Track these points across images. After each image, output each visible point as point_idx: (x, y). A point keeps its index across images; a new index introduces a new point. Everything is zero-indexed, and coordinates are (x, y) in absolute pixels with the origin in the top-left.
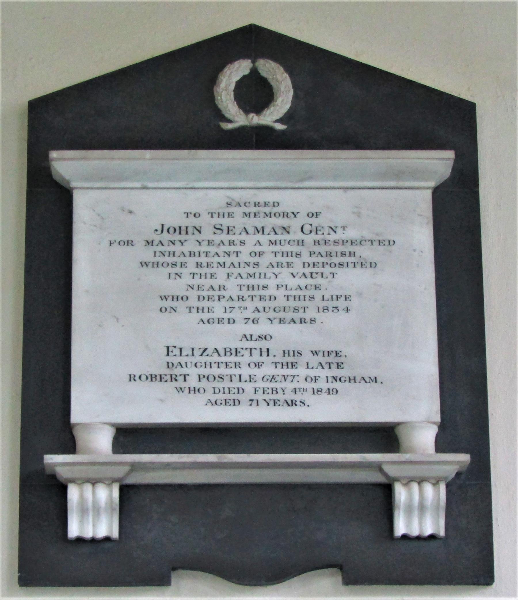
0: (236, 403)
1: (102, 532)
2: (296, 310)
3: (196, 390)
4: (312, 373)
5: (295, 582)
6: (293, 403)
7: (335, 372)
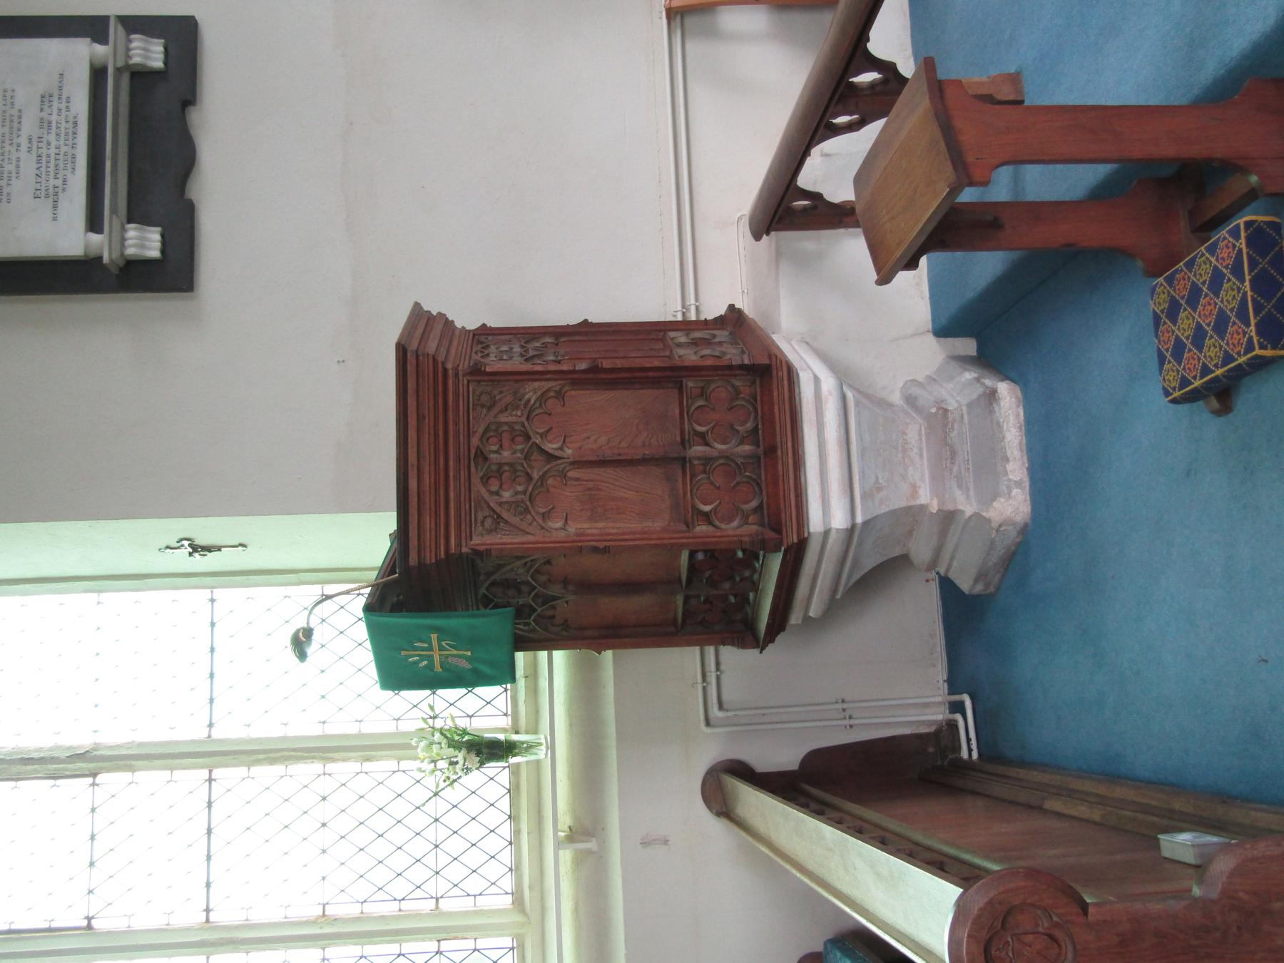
0: (74, 157)
1: (157, 237)
2: (12, 121)
3: (65, 181)
4: (55, 111)
5: (193, 133)
6: (75, 123)
7: (55, 99)
